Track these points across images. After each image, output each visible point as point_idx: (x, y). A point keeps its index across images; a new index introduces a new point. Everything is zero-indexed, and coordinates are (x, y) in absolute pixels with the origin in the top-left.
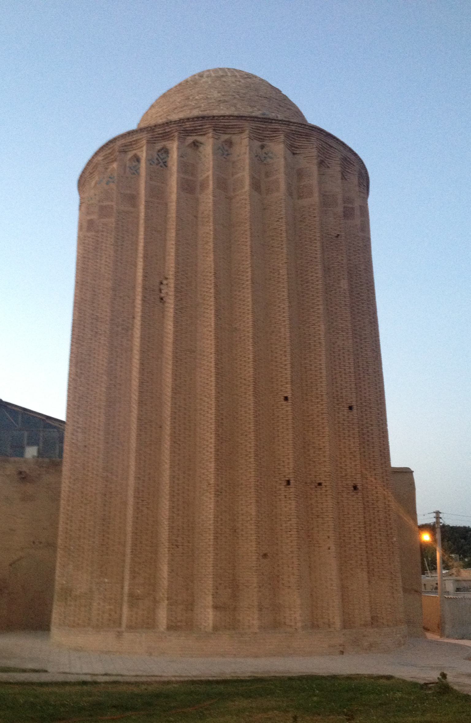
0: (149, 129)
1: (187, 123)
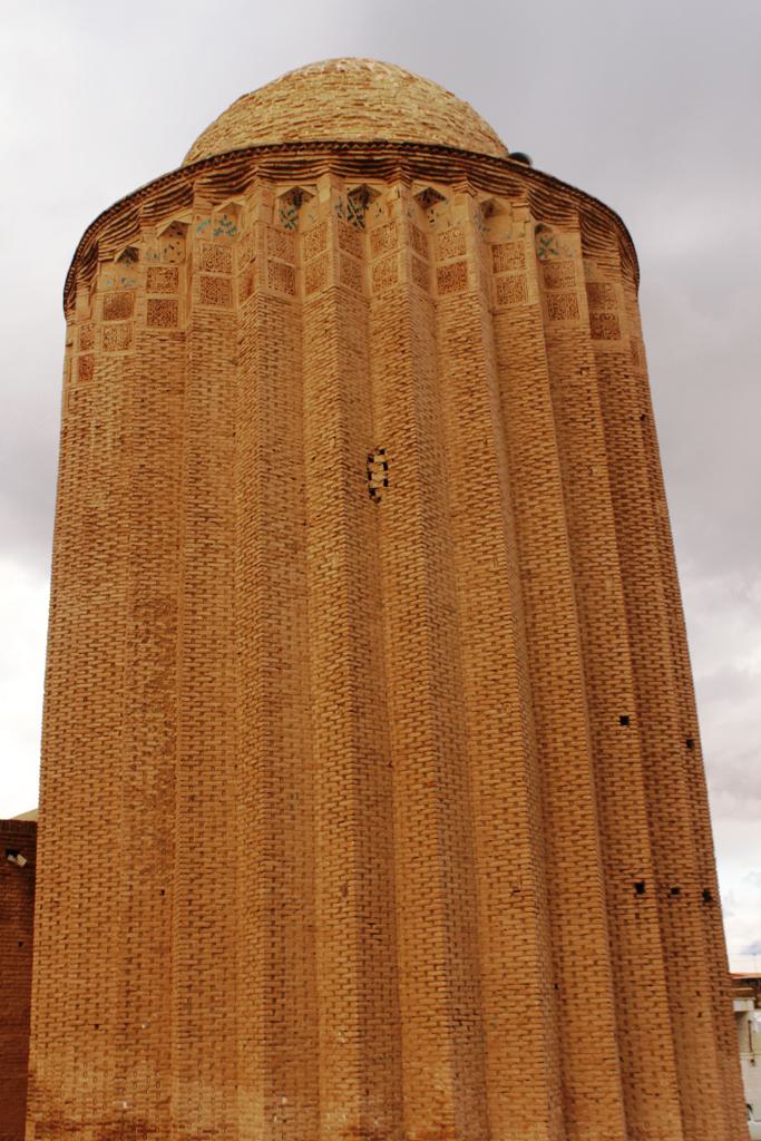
0: (337, 146)
1: (418, 154)
